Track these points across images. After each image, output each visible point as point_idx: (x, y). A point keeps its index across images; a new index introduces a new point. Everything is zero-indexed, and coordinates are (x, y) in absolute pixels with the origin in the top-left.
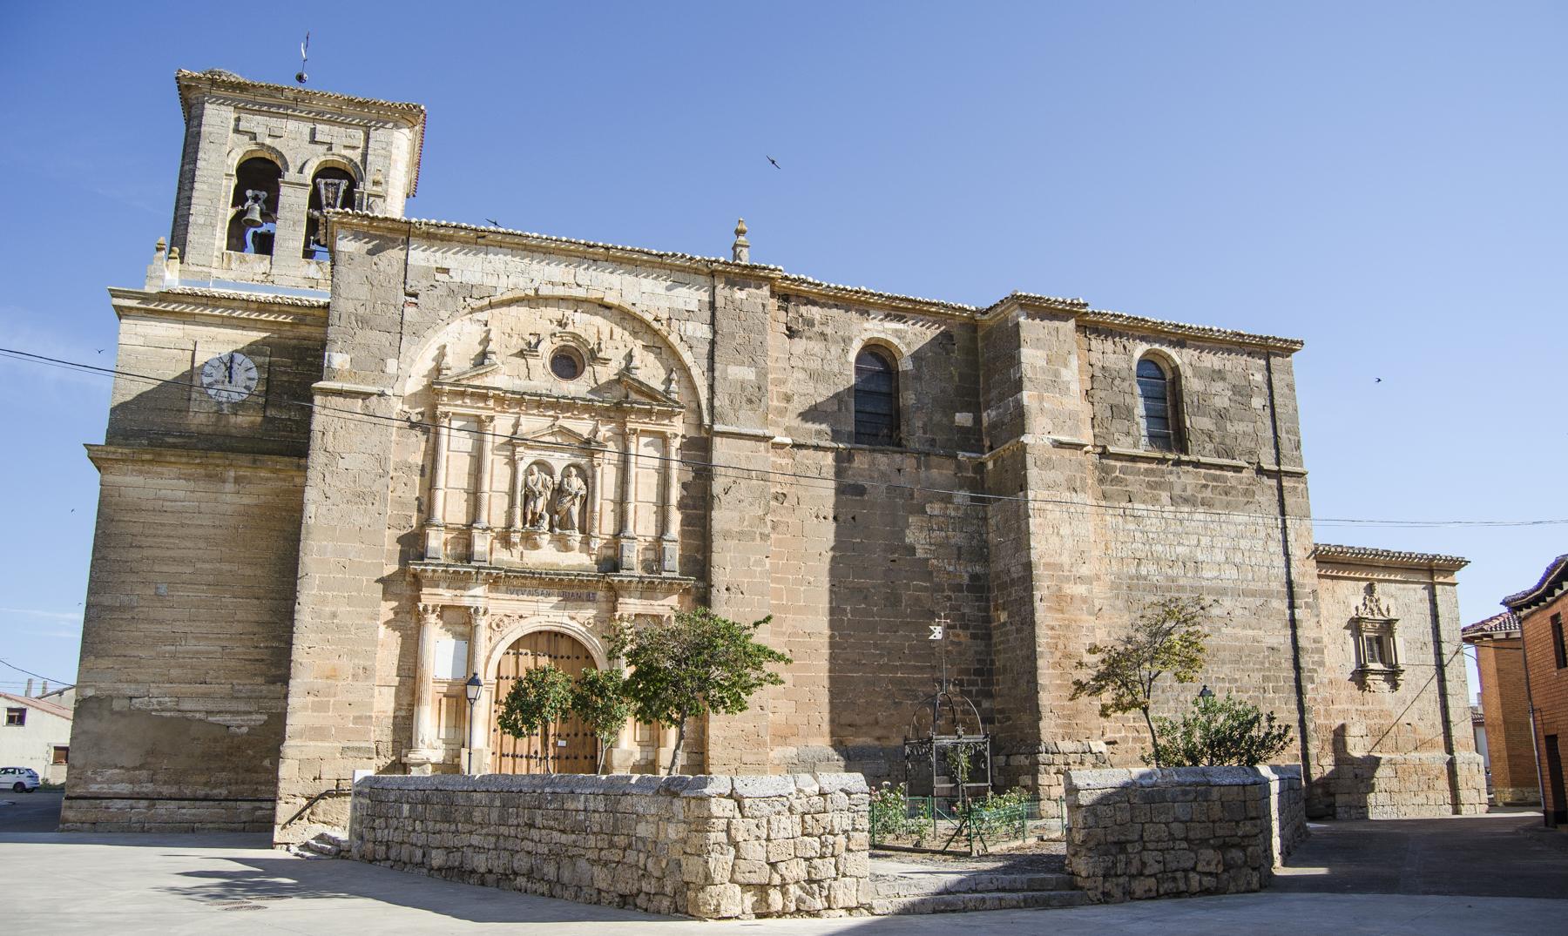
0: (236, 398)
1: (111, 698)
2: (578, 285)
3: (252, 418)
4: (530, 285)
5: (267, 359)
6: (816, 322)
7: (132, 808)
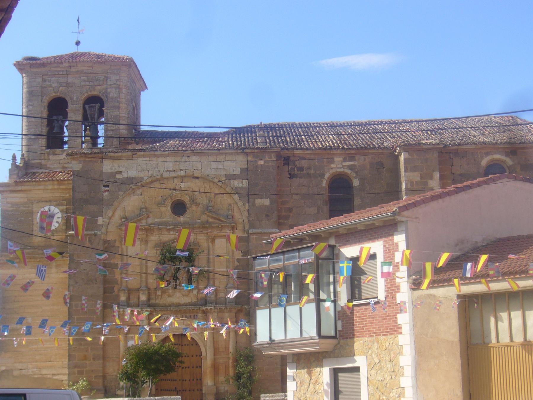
4: (158, 174)
5: (65, 207)
6: (304, 168)
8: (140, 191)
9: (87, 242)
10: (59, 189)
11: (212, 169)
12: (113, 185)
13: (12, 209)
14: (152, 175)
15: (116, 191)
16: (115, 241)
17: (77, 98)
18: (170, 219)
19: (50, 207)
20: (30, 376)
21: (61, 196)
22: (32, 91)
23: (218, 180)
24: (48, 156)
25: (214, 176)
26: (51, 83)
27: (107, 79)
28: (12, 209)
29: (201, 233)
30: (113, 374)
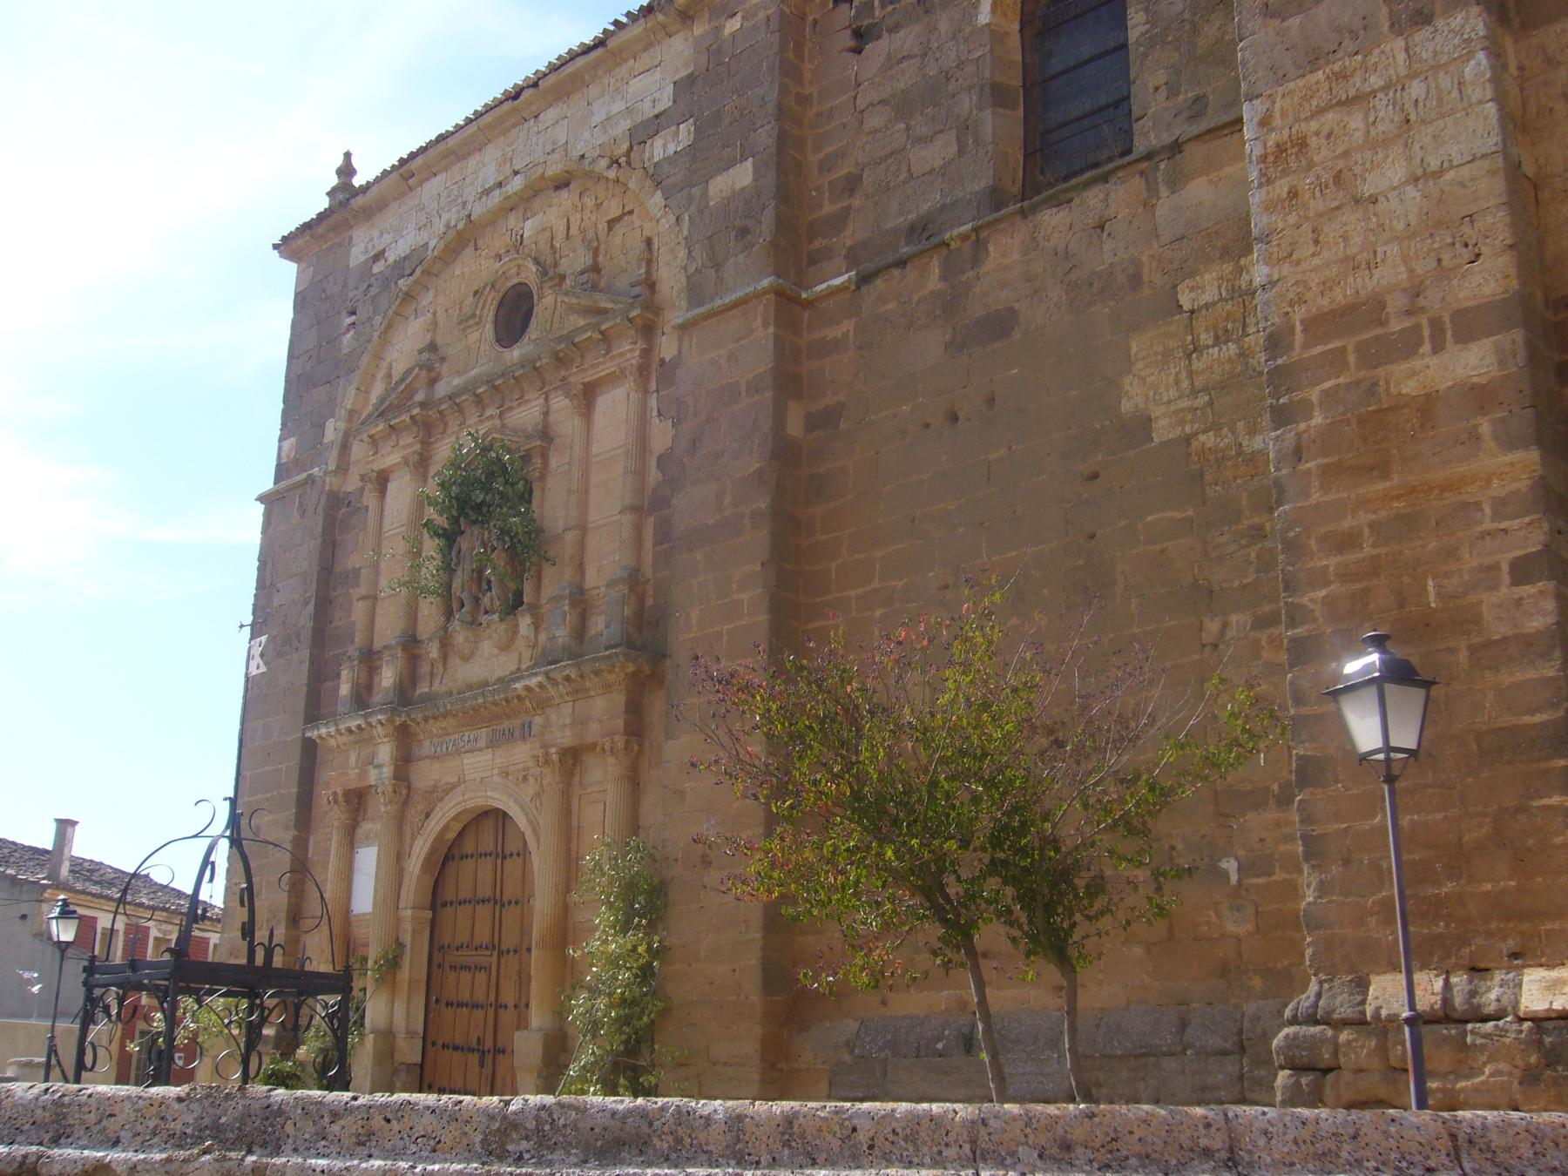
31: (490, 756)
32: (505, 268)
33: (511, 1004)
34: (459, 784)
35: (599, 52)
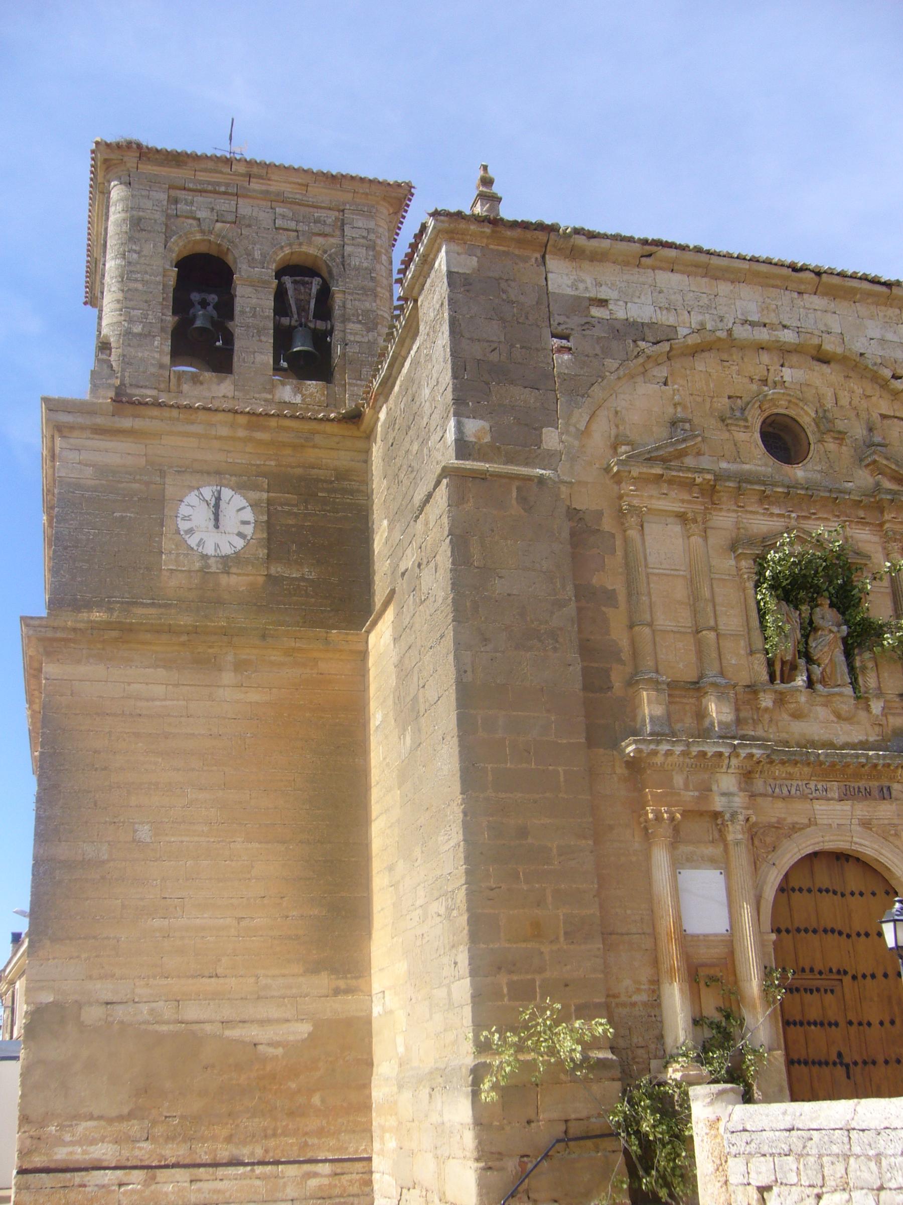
0: (227, 550)
1: (79, 1005)
2: (785, 327)
3: (251, 578)
4: (720, 325)
5: (265, 495)
7: (120, 1185)
8: (662, 372)
9: (514, 502)
10: (250, 439)
11: (871, 339)
12: (584, 335)
13: (97, 482)
14: (701, 328)
15: (596, 355)
16: (599, 514)
17: (264, 256)
18: (763, 468)
19: (219, 492)
20: (143, 1027)
21: (253, 462)
22: (140, 219)
23: (890, 374)
24: (179, 385)
25: (879, 361)
26: (193, 208)
27: (342, 225)
28: (97, 482)
29: (862, 522)
30: (635, 998)
31: (848, 808)
32: (775, 396)
33: (875, 1022)
34: (809, 826)
35: (884, 289)
